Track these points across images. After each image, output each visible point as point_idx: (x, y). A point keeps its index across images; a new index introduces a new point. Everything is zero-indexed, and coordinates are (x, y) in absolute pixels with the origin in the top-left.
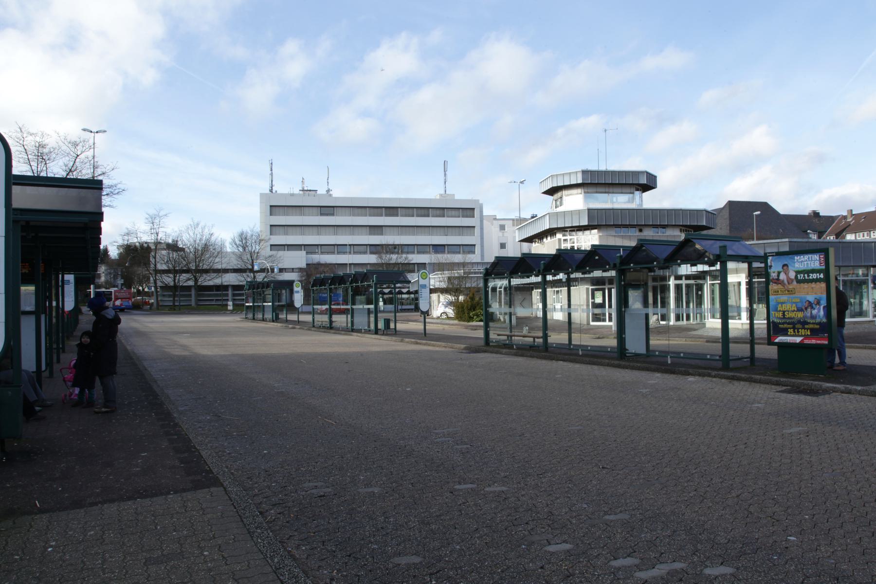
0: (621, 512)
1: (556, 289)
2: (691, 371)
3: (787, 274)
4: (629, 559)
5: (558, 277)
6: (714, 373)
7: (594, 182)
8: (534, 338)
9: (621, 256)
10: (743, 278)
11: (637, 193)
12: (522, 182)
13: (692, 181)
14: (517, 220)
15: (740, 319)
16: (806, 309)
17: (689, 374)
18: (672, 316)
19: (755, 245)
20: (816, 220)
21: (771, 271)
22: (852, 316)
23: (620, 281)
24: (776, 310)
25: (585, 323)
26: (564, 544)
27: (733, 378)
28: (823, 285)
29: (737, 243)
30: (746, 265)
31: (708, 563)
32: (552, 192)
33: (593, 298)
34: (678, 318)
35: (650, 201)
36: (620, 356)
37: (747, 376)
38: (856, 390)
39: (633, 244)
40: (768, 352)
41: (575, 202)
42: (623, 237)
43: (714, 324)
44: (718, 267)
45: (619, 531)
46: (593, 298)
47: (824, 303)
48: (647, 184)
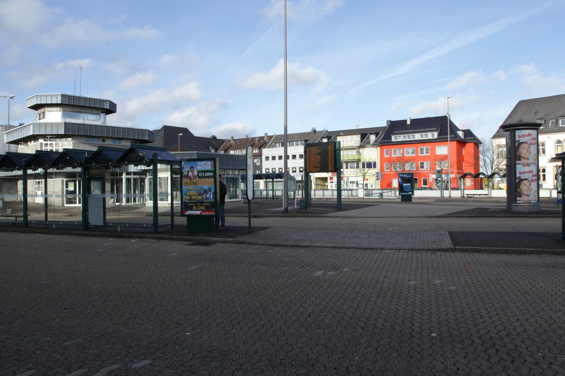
0: (76, 338)
1: (39, 180)
2: (133, 235)
3: (193, 172)
4: (80, 370)
5: (37, 172)
6: (148, 236)
7: (70, 104)
8: (16, 217)
9: (86, 158)
10: (168, 175)
11: (102, 115)
12: (12, 98)
13: (140, 110)
14: (5, 126)
15: (167, 201)
16: (203, 194)
17: (131, 237)
18: (124, 199)
19: (177, 154)
20: (214, 141)
21: (183, 170)
22: (231, 198)
23: (85, 175)
24: (186, 195)
25: (61, 205)
26: (29, 371)
27: (160, 238)
28: (213, 180)
29: (164, 153)
30: (169, 167)
31: (135, 360)
32: (36, 107)
33: (67, 187)
34: (128, 201)
35: (111, 120)
36: (84, 228)
37: (169, 236)
38: (229, 241)
39: (95, 149)
40: (181, 221)
41: (55, 116)
42: (90, 144)
43: (150, 203)
44: (151, 167)
45: (74, 352)
46: (67, 187)
47: (213, 190)
48: (111, 109)
